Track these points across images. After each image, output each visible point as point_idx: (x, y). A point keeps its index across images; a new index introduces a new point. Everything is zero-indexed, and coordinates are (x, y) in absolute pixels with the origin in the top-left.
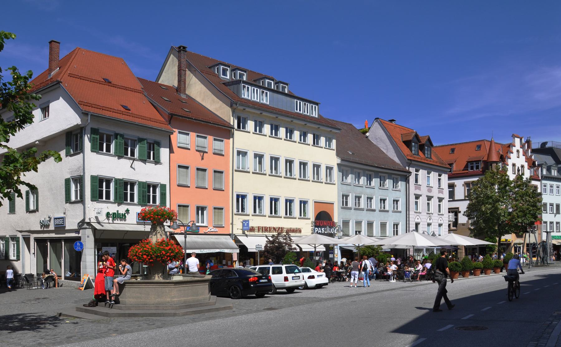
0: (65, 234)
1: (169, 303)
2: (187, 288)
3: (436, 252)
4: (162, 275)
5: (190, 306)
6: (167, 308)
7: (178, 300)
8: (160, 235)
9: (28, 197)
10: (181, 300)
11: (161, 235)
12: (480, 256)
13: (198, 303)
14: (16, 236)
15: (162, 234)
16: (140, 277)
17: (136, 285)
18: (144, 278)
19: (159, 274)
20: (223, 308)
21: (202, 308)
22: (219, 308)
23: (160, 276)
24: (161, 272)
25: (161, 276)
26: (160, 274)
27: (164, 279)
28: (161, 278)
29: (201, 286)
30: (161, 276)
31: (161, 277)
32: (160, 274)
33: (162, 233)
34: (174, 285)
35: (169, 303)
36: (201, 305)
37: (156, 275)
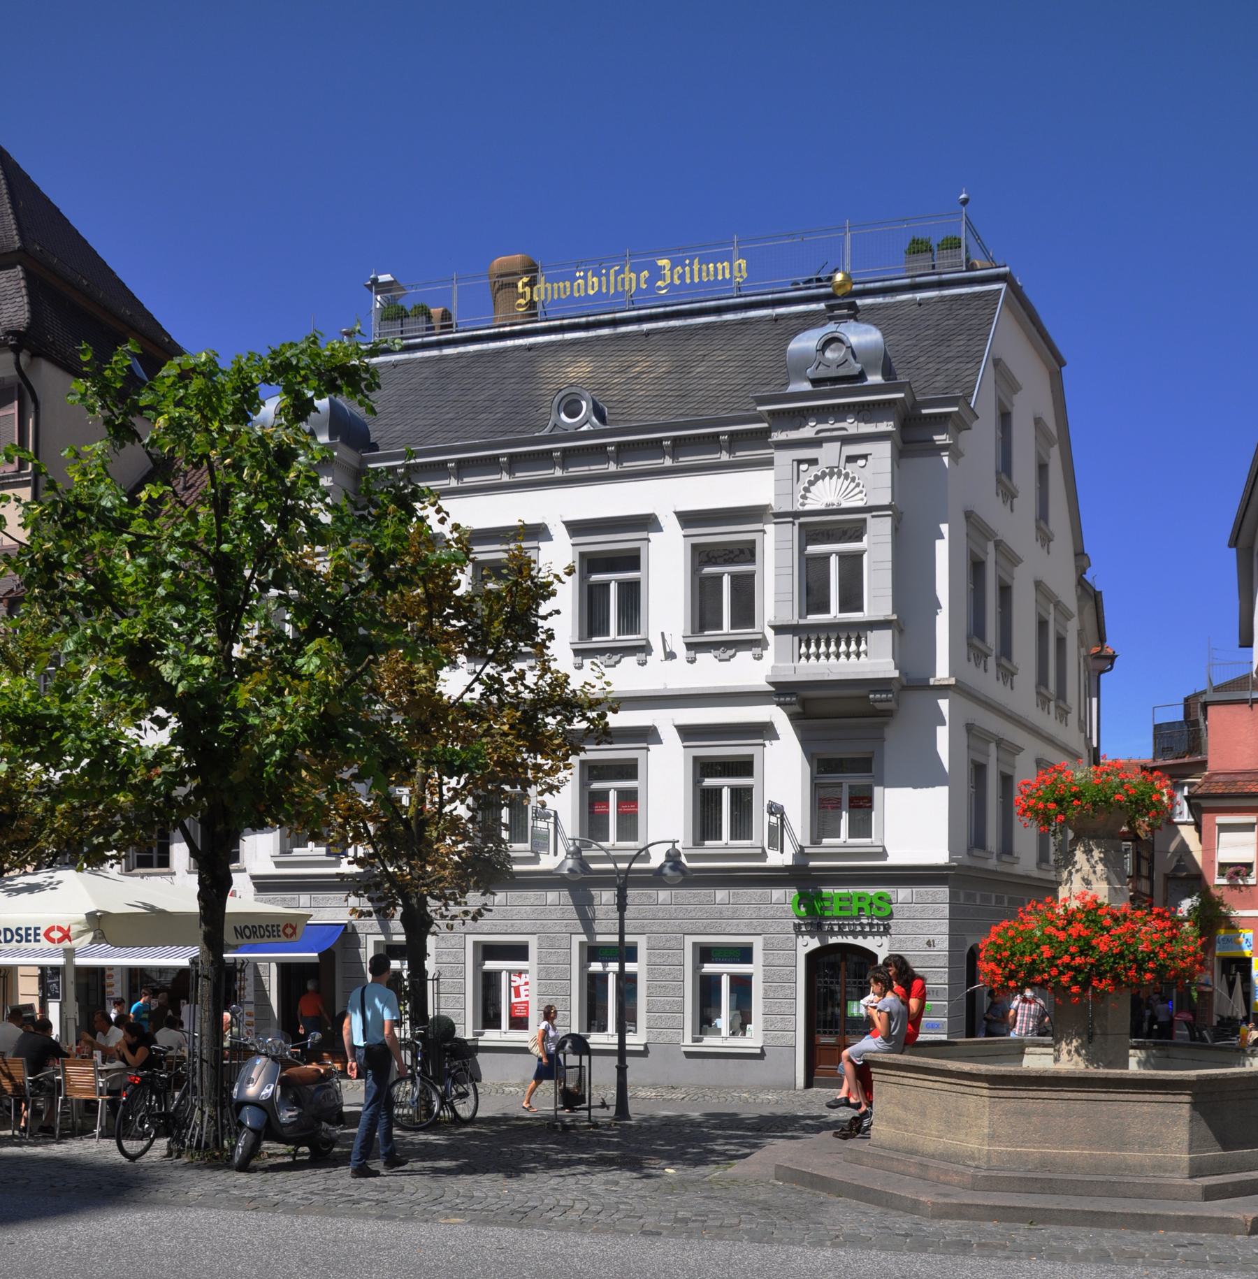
0: (77, 999)
1: (973, 1159)
2: (1062, 1106)
3: (179, 1013)
4: (1082, 1046)
5: (1048, 1186)
6: (948, 1178)
7: (1009, 1153)
8: (1084, 879)
9: (631, 808)
10: (1027, 1154)
11: (1087, 882)
12: (431, 1017)
13: (1101, 1178)
14: (883, 855)
15: (1092, 878)
16: (1138, 1051)
17: (893, 1072)
18: (1154, 1056)
19: (1071, 1042)
20: (1179, 1217)
21: (1104, 1205)
22: (1155, 1216)
23: (1073, 1049)
24: (1079, 1035)
25: (1077, 1051)
26: (1075, 1043)
27: (1091, 1060)
28: (1076, 1057)
29: (1146, 1108)
30: (1077, 1051)
31: (1079, 1055)
32: (1075, 1043)
33: (1094, 872)
34: (987, 1085)
35: (973, 1159)
36: (1145, 1193)
37: (1064, 1043)
